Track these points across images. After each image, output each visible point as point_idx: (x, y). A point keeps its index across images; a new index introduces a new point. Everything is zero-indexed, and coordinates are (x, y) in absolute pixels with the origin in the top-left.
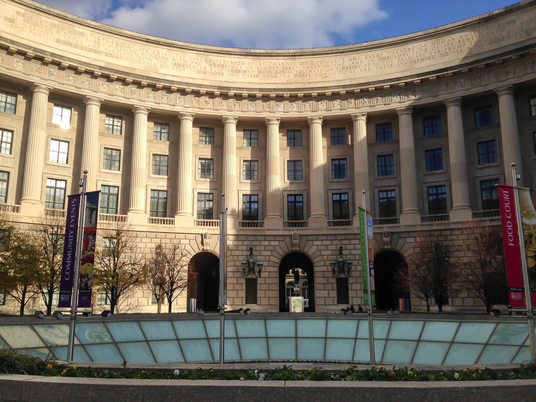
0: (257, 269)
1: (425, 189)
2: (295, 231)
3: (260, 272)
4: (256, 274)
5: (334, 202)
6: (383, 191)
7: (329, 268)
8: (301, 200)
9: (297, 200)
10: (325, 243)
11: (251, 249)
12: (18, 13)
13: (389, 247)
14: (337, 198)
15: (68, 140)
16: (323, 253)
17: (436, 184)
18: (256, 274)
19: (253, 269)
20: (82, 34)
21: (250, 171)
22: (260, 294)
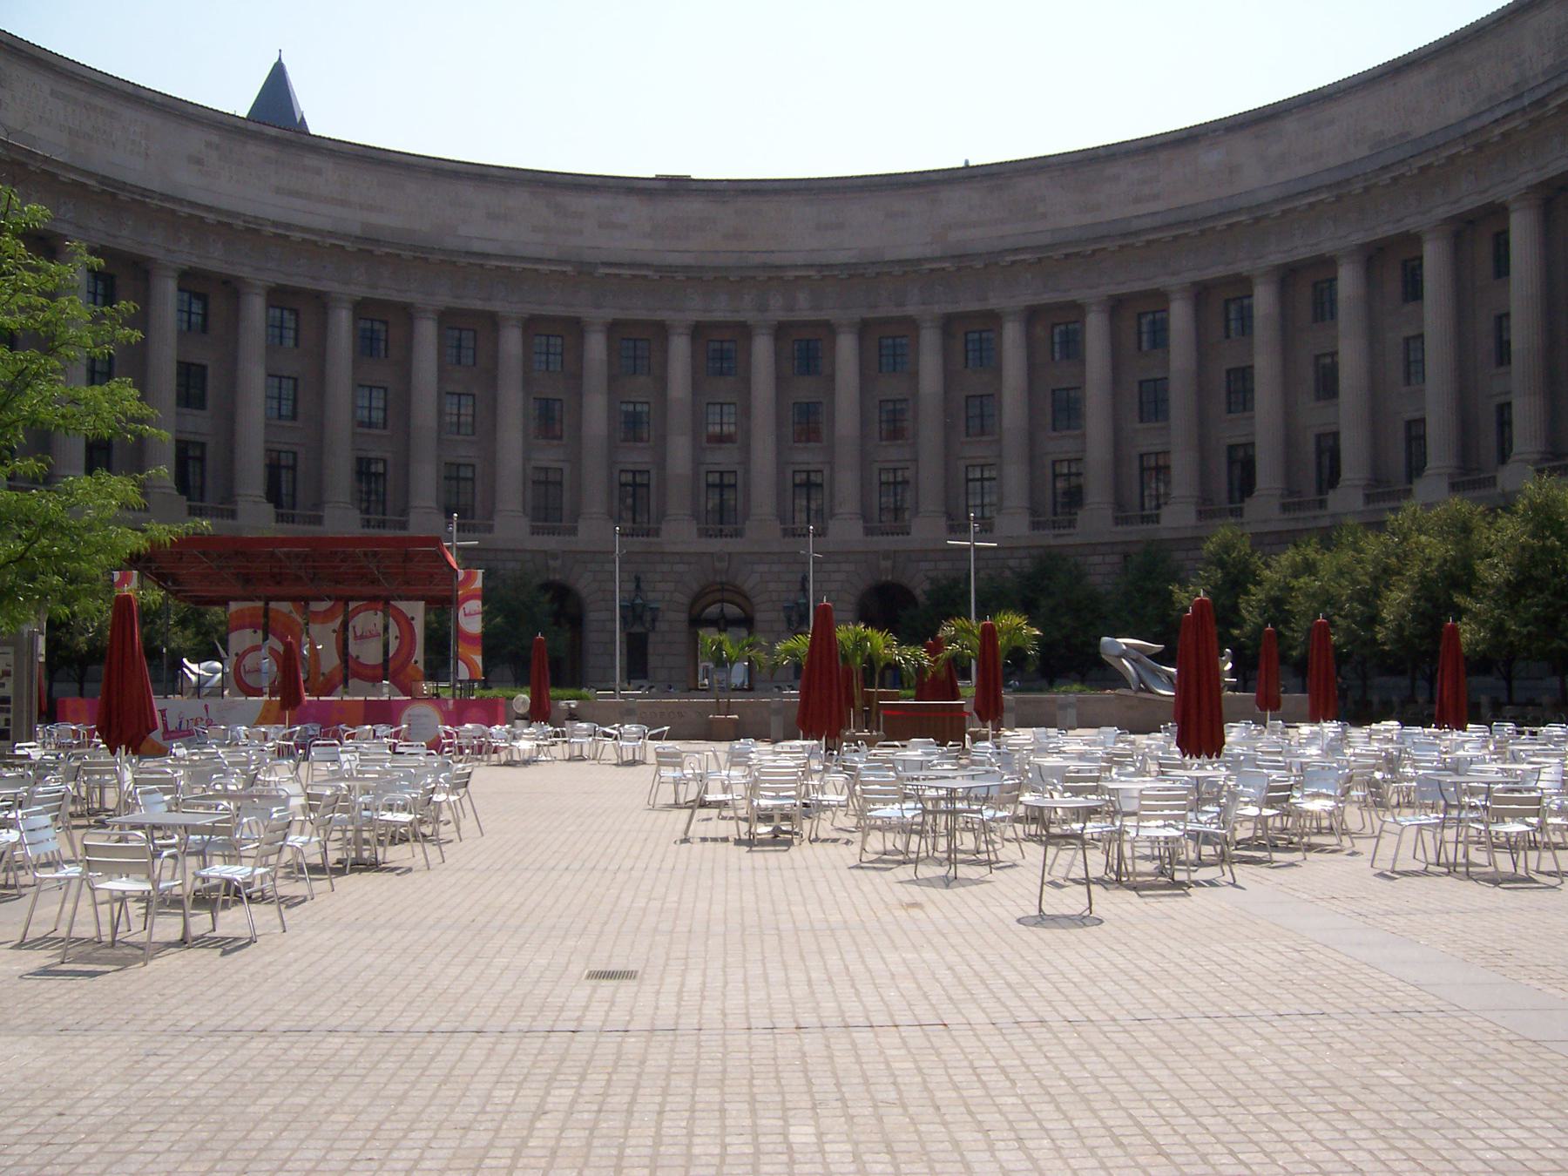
0: (648, 617)
1: (789, 473)
2: (716, 545)
3: (654, 620)
4: (647, 625)
5: (623, 485)
6: (887, 470)
7: (782, 614)
8: (733, 482)
9: (726, 481)
10: (775, 568)
11: (638, 580)
12: (209, 145)
13: (890, 578)
14: (628, 478)
15: (295, 375)
16: (772, 586)
17: (982, 461)
18: (647, 625)
19: (641, 618)
20: (318, 172)
21: (1242, 318)
22: (653, 660)
